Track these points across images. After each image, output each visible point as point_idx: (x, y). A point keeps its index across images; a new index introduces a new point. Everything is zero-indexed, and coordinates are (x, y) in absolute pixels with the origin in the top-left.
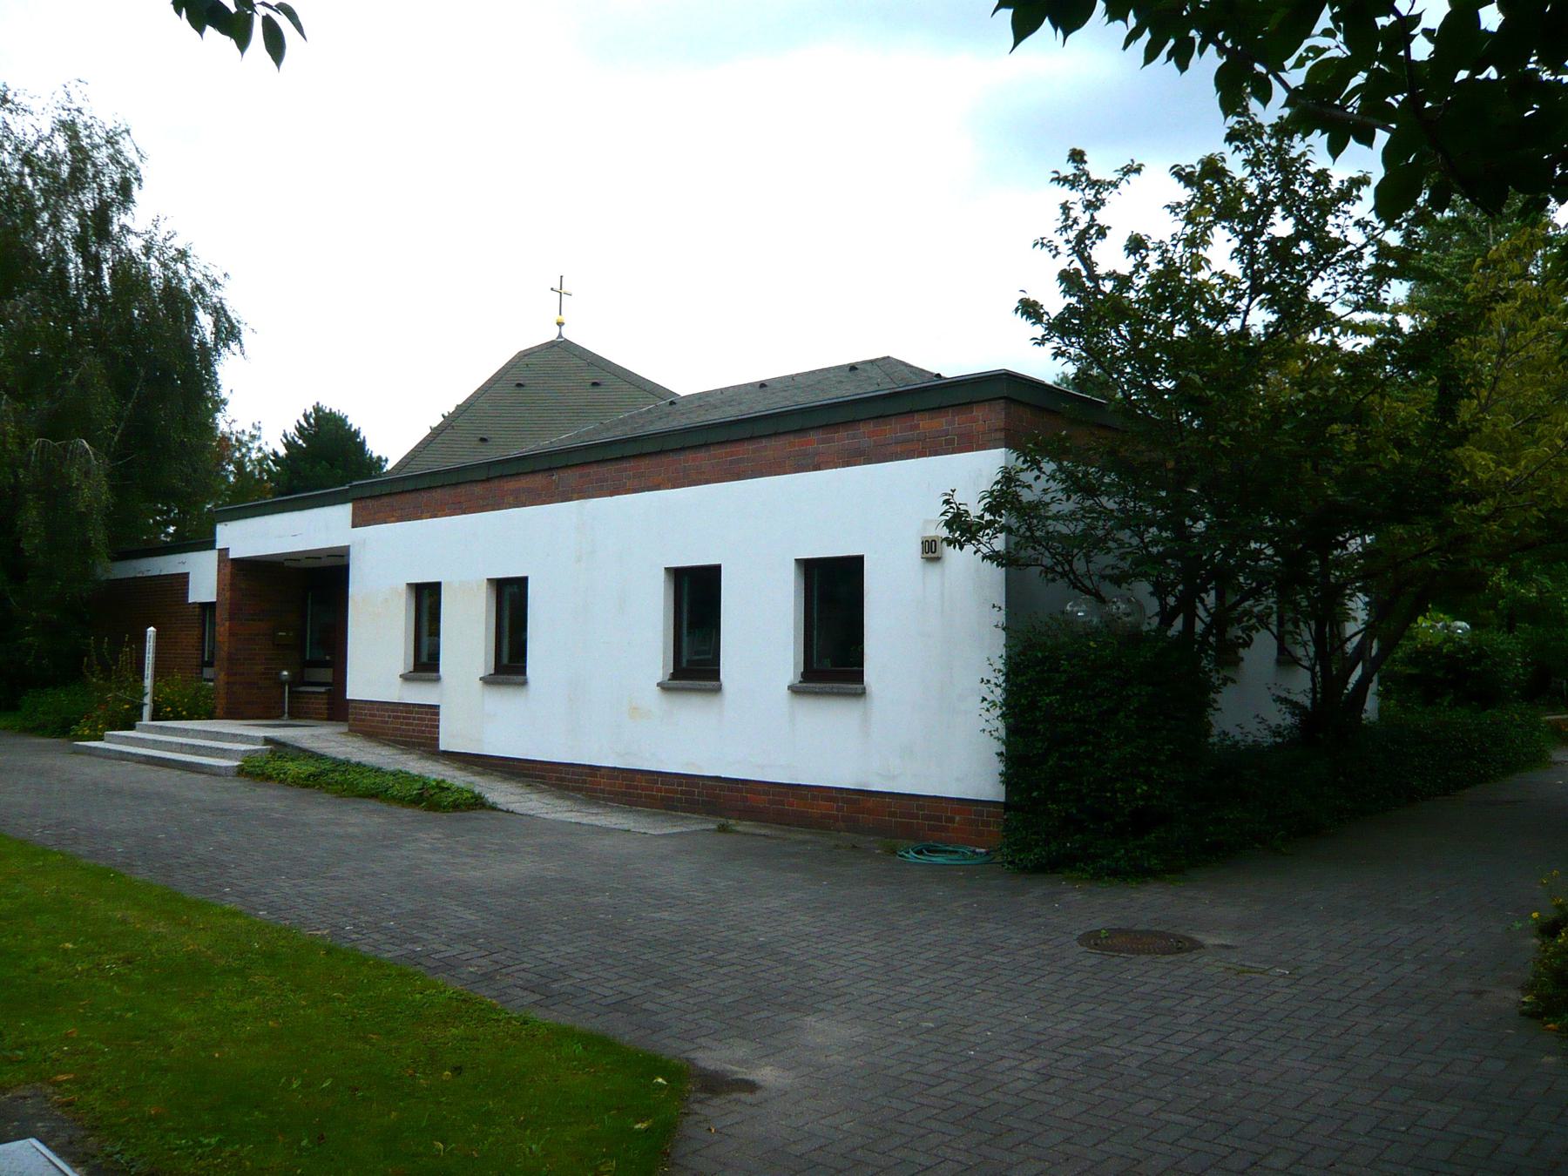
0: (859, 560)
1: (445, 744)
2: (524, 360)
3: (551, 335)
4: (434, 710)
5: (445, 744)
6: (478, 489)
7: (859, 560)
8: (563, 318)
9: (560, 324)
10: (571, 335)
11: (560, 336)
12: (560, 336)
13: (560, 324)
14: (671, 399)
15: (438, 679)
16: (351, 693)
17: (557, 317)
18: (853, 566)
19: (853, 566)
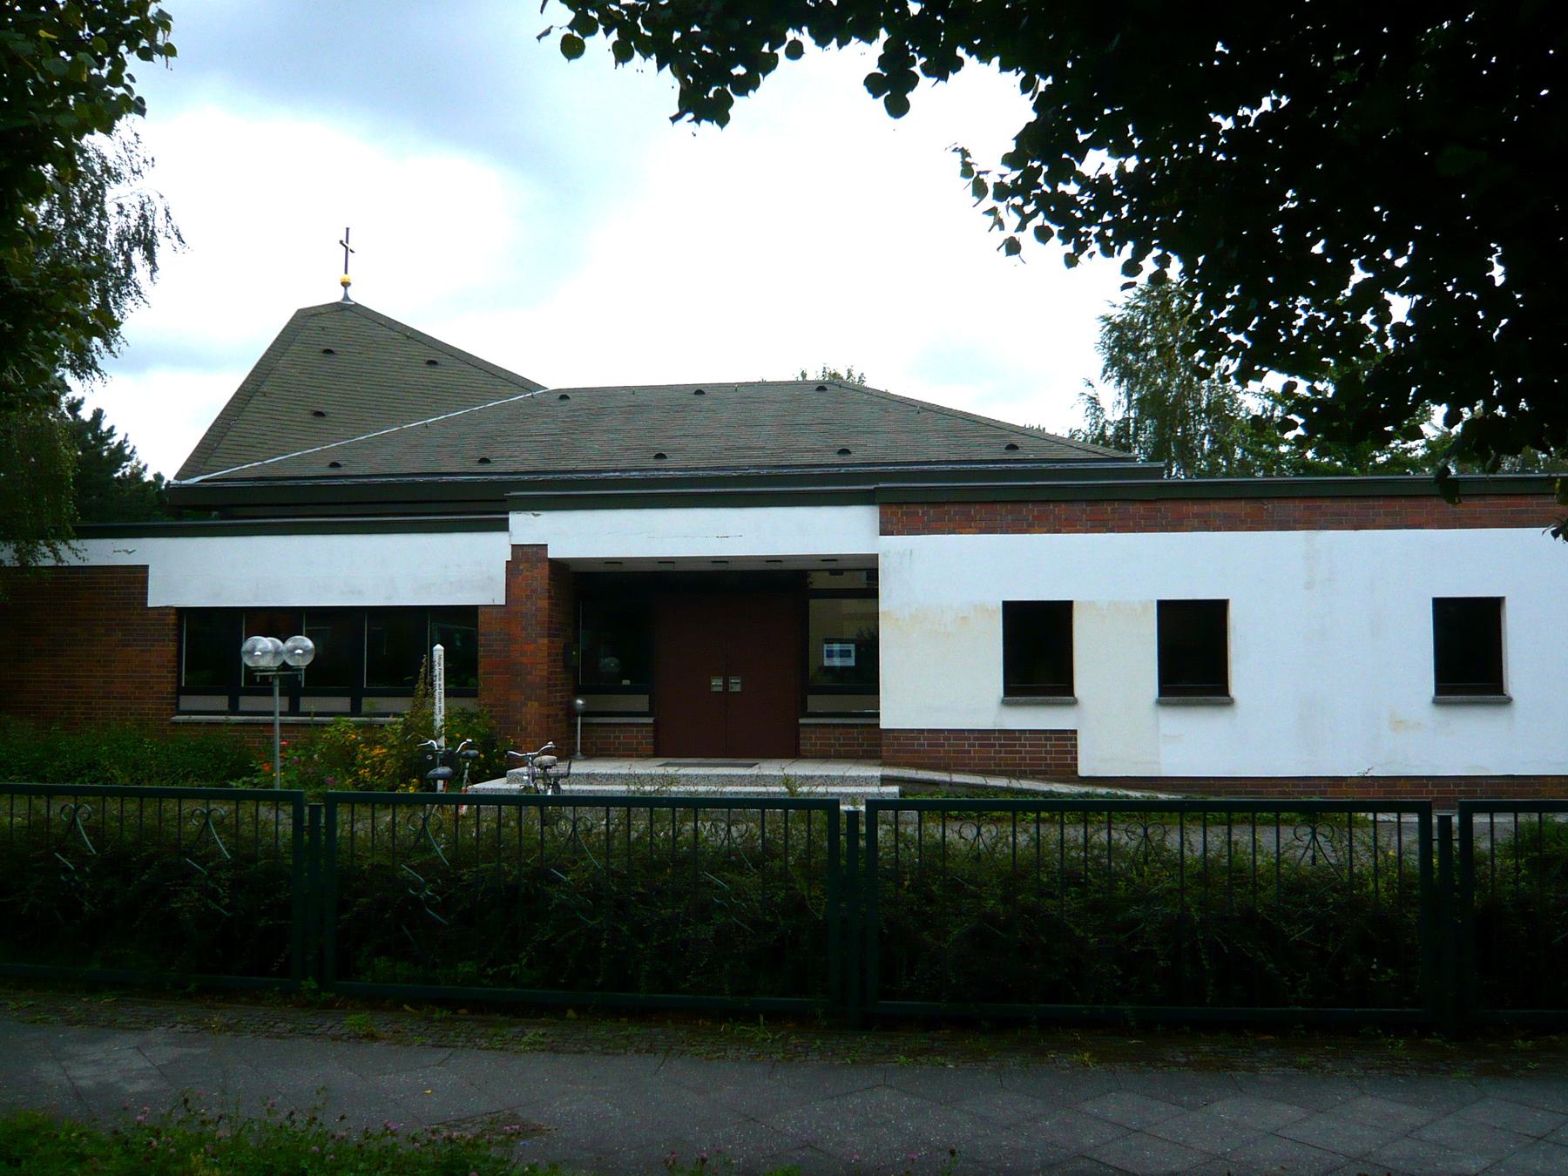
0: (1439, 604)
1: (1084, 770)
2: (304, 319)
3: (336, 296)
4: (1069, 736)
5: (1084, 770)
6: (1141, 509)
7: (1439, 604)
8: (350, 277)
9: (345, 284)
10: (357, 296)
11: (346, 297)
12: (346, 297)
13: (345, 284)
14: (1055, 440)
15: (1075, 703)
16: (886, 723)
17: (342, 276)
18: (1215, 612)
19: (1215, 612)
